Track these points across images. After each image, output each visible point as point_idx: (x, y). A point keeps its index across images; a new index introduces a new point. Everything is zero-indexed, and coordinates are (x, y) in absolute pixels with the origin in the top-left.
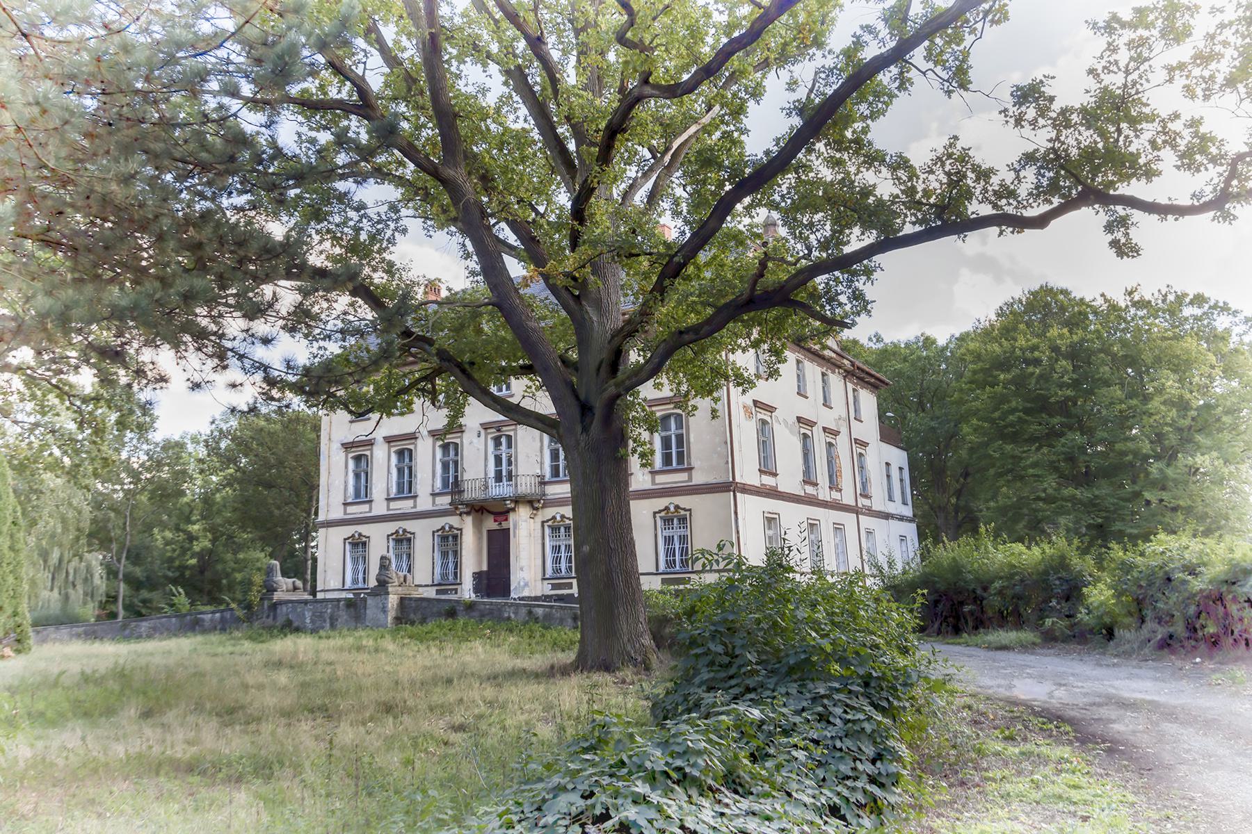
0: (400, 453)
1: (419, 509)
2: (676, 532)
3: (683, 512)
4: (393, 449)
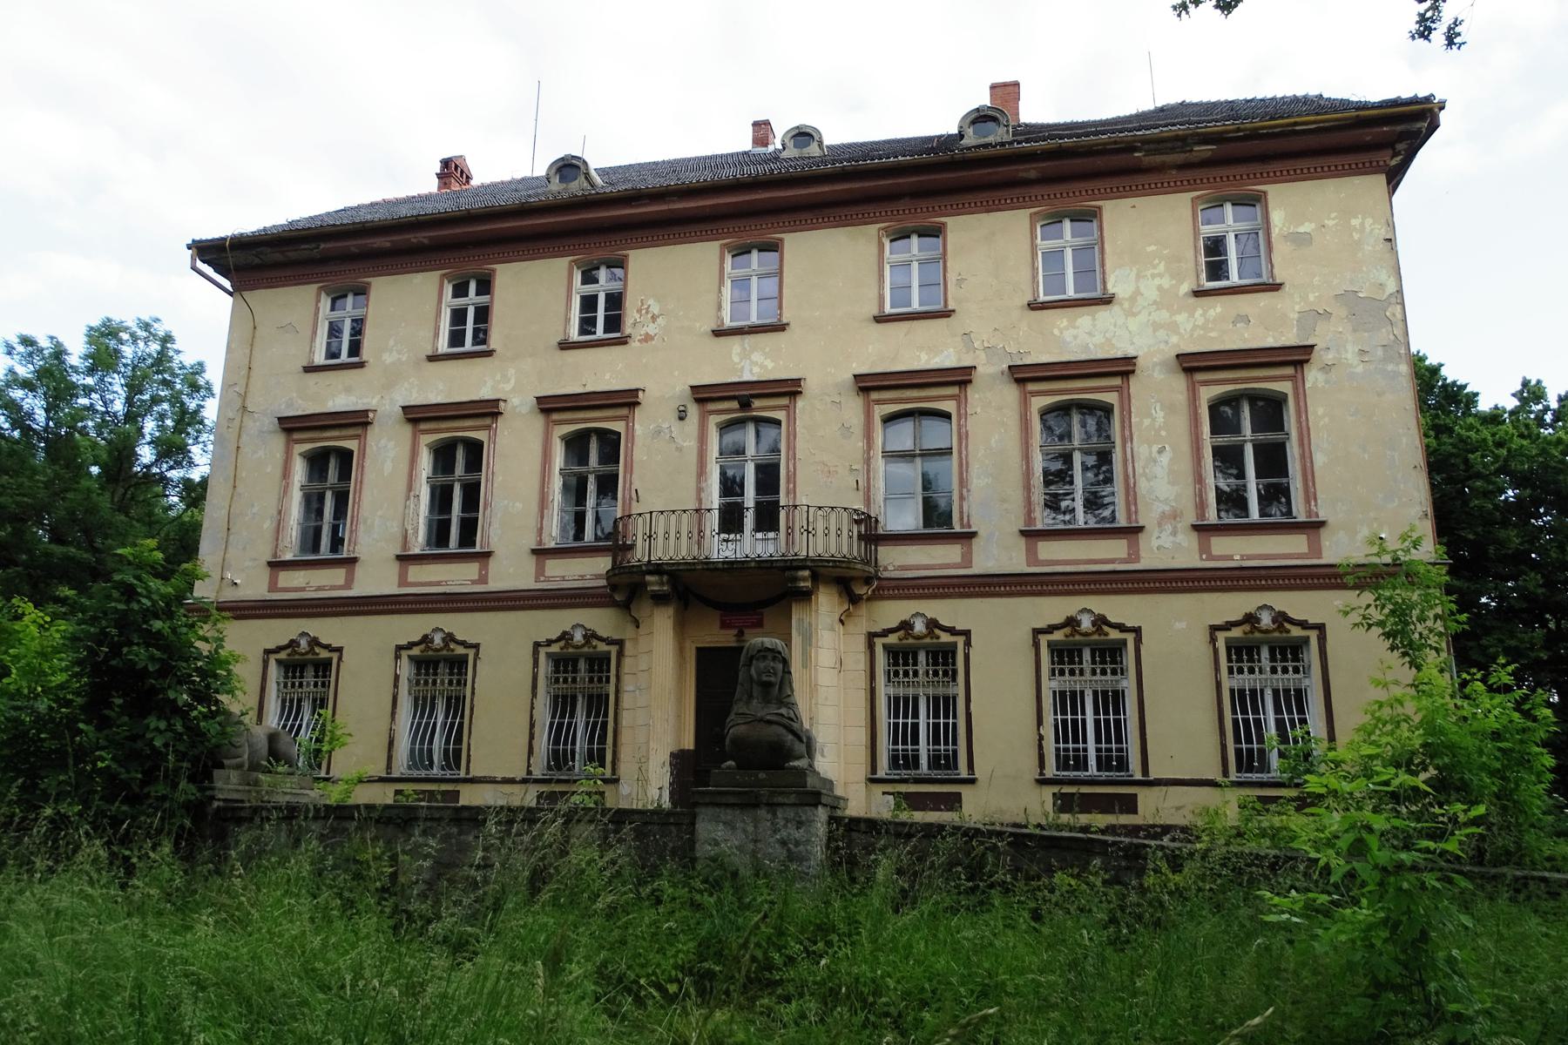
0: (317, 462)
1: (494, 585)
2: (1088, 682)
3: (602, 647)
4: (426, 439)
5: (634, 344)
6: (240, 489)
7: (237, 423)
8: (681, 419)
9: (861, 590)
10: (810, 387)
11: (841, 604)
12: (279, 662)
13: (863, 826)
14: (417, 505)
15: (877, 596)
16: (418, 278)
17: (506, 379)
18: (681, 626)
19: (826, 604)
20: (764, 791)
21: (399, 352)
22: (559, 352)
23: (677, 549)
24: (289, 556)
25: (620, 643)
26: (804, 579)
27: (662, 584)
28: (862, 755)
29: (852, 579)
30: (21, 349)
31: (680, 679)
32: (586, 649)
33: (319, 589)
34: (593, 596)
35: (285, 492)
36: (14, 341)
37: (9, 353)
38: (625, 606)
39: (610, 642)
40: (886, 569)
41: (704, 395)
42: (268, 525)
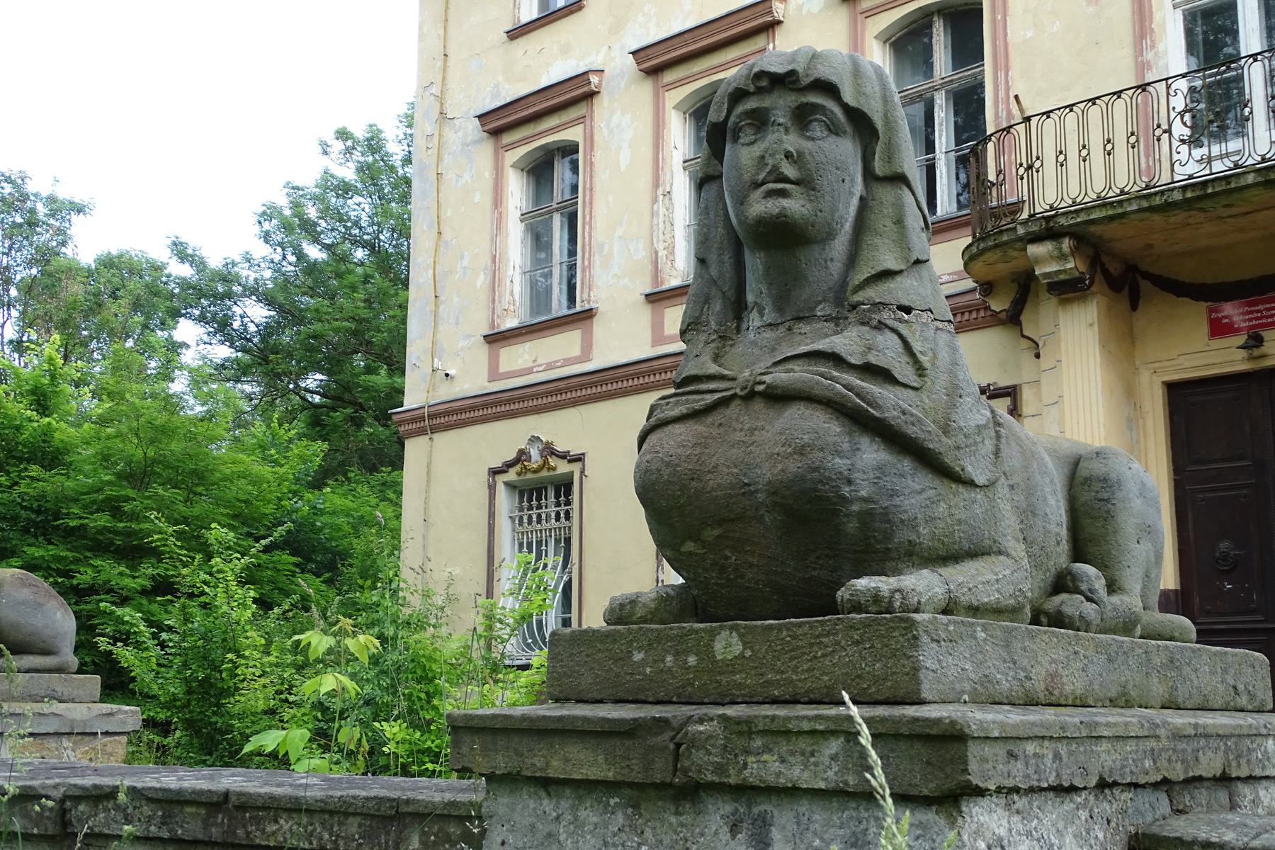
4: (675, 97)
6: (447, 235)
12: (506, 484)
18: (1123, 343)
20: (706, 723)
24: (511, 323)
25: (1011, 393)
27: (1062, 257)
30: (338, 146)
33: (550, 367)
35: (499, 228)
36: (329, 137)
37: (325, 153)
38: (1012, 319)
42: (482, 281)
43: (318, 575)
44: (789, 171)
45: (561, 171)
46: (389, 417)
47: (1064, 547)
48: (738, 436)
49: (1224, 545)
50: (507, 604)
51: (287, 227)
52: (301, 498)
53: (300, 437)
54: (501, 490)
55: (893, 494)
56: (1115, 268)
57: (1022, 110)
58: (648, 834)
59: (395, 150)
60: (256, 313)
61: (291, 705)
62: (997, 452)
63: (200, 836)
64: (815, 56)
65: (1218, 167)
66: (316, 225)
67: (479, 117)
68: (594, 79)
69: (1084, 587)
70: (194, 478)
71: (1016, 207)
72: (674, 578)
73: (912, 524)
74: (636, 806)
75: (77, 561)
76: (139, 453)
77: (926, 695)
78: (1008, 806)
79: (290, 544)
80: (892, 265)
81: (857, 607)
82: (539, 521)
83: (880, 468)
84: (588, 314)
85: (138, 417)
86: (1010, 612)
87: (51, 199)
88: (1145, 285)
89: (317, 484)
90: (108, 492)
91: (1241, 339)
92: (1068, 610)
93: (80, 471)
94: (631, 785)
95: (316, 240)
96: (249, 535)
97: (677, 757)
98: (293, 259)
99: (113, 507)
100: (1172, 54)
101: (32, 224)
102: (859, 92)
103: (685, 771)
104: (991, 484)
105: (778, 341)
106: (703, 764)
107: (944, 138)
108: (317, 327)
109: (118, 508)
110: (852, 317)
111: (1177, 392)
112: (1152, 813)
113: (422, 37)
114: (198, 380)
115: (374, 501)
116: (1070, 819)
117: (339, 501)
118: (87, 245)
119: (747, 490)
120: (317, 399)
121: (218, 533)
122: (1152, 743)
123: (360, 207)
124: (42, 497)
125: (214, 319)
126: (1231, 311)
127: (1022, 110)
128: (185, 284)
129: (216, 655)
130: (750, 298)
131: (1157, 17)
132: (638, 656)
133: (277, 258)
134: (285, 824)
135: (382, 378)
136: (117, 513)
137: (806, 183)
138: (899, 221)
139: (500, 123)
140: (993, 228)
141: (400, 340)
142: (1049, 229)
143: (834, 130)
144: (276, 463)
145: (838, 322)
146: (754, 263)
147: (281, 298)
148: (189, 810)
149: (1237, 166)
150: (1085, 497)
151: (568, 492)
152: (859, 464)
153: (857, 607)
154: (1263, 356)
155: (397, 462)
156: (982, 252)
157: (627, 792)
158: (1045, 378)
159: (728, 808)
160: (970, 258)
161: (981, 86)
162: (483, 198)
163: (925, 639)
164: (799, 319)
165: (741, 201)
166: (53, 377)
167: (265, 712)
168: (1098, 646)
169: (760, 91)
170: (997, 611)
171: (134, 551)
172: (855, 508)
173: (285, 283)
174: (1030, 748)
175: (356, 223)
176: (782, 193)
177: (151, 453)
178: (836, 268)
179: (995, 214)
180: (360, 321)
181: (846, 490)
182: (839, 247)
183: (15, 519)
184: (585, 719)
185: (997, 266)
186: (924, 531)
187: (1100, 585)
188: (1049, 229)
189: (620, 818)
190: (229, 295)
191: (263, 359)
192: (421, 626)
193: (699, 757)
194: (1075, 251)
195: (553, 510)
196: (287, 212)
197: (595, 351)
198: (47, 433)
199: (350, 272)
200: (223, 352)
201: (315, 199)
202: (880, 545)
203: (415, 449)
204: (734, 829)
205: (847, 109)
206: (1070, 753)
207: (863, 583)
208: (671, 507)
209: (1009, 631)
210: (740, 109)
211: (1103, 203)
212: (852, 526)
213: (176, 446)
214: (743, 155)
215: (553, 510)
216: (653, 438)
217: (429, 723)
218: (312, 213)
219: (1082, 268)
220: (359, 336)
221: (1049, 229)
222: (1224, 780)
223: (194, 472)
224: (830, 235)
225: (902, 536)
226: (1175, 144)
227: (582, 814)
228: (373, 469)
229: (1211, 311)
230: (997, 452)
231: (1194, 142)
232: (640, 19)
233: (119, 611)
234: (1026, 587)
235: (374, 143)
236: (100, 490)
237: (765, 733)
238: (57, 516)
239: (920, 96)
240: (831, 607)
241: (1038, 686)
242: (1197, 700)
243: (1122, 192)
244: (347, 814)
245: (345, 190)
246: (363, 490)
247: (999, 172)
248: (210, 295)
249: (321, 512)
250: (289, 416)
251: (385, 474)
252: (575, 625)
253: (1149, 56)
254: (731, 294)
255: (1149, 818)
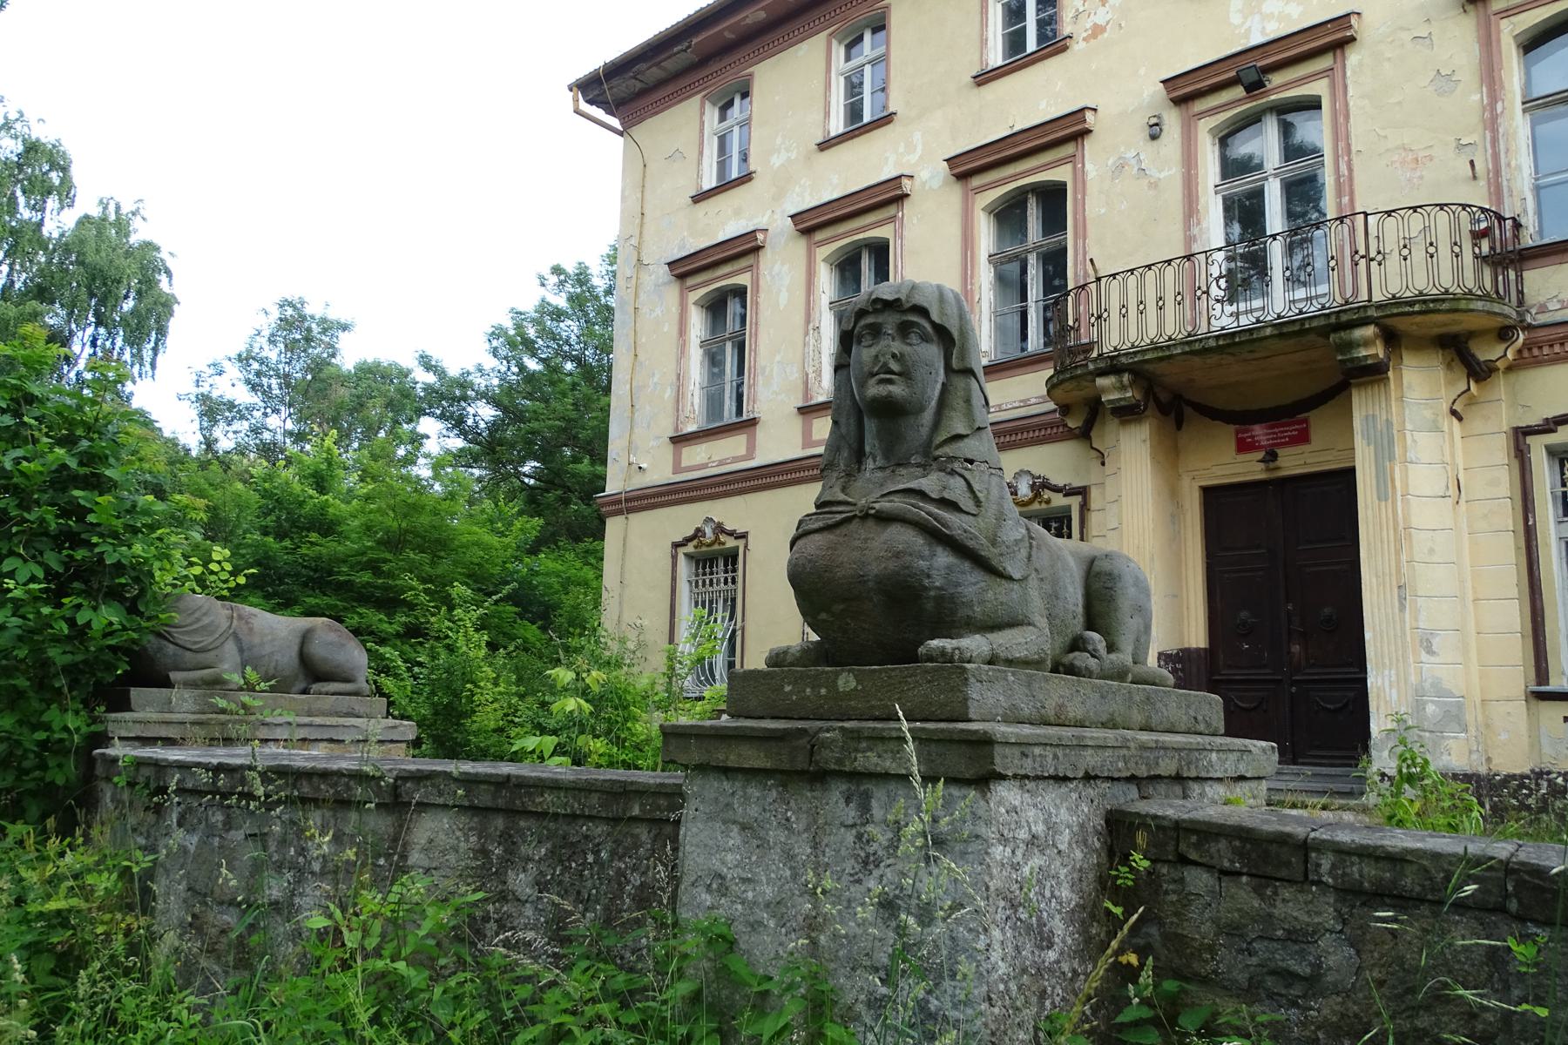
3: (1058, 500)
5: (1077, 47)
7: (634, 281)
8: (1154, 137)
9: (1488, 352)
10: (1368, 29)
11: (1450, 383)
12: (688, 556)
13: (1222, 852)
14: (818, 340)
15: (1527, 360)
16: (804, 46)
17: (910, 147)
18: (1169, 455)
19: (1420, 386)
20: (830, 732)
21: (787, 150)
22: (976, 90)
23: (1142, 327)
24: (691, 428)
25: (1083, 492)
26: (1367, 343)
27: (1123, 388)
28: (1516, 650)
29: (1471, 334)
30: (554, 279)
31: (1174, 540)
32: (1036, 506)
33: (721, 463)
34: (1040, 427)
35: (683, 352)
36: (546, 272)
38: (1084, 434)
39: (1069, 492)
40: (1543, 309)
41: (1186, 91)
42: (669, 394)
43: (533, 623)
44: (894, 366)
45: (733, 307)
46: (590, 498)
47: (1080, 619)
48: (857, 543)
49: (1244, 614)
50: (686, 648)
51: (511, 344)
52: (521, 561)
53: (520, 513)
54: (682, 560)
55: (958, 585)
56: (1164, 397)
57: (1095, 271)
58: (792, 803)
59: (599, 283)
60: (485, 413)
61: (516, 725)
62: (1029, 557)
63: (489, 804)
64: (914, 287)
65: (1245, 321)
66: (534, 342)
67: (669, 264)
68: (760, 236)
69: (1090, 648)
70: (437, 544)
71: (1089, 347)
72: (814, 637)
73: (970, 605)
74: (784, 786)
75: (345, 609)
76: (395, 524)
77: (972, 715)
78: (1021, 787)
79: (512, 598)
80: (962, 431)
81: (931, 659)
82: (711, 584)
83: (949, 568)
84: (753, 422)
85: (394, 496)
86: (1036, 664)
87: (324, 320)
88: (1188, 411)
89: (533, 550)
90: (370, 555)
91: (1260, 455)
92: (1077, 663)
93: (347, 538)
94: (782, 772)
95: (534, 355)
96: (480, 590)
97: (812, 753)
98: (515, 370)
99: (374, 567)
100: (1214, 229)
101: (308, 340)
102: (942, 313)
103: (817, 763)
104: (1025, 579)
105: (885, 479)
106: (829, 759)
107: (1035, 291)
108: (535, 425)
109: (379, 568)
110: (935, 466)
111: (1211, 495)
112: (1128, 799)
113: (623, 198)
114: (437, 466)
115: (578, 564)
116: (1064, 798)
117: (551, 565)
118: (350, 355)
119: (861, 580)
120: (532, 482)
121: (459, 590)
122: (1124, 751)
123: (570, 328)
124: (319, 558)
125: (452, 417)
126: (1259, 432)
127: (1095, 271)
128: (428, 389)
129: (457, 685)
130: (867, 449)
131: (1202, 201)
132: (788, 688)
133: (503, 369)
134: (548, 797)
135: (585, 466)
136: (377, 571)
137: (906, 375)
138: (968, 401)
139: (685, 269)
140: (1069, 360)
141: (603, 437)
142: (1113, 366)
143: (925, 338)
144: (502, 534)
145: (925, 468)
146: (870, 426)
147: (506, 401)
148: (483, 787)
149: (1258, 321)
150: (1097, 585)
151: (735, 562)
152: (936, 565)
153: (931, 659)
154: (1278, 468)
155: (599, 535)
156: (1061, 382)
157: (779, 776)
158: (1109, 481)
159: (844, 787)
160: (1052, 386)
161: (1065, 250)
162: (670, 328)
163: (972, 680)
164: (899, 465)
165: (862, 385)
166: (330, 464)
167: (494, 731)
168: (1094, 687)
169: (876, 311)
170: (1026, 663)
171: (390, 602)
172: (932, 593)
173: (509, 389)
174: (1037, 751)
175: (567, 342)
176: (890, 382)
177: (404, 525)
178: (925, 431)
179: (1072, 352)
180: (570, 420)
181: (926, 582)
182: (927, 417)
183: (297, 575)
184: (752, 729)
185: (1073, 393)
186: (977, 609)
187: (1101, 646)
188: (1113, 366)
189: (774, 793)
190: (465, 398)
191: (489, 448)
192: (619, 665)
193: (826, 753)
194: (1132, 384)
195: (722, 576)
196: (512, 332)
197: (758, 452)
198: (324, 507)
199: (561, 381)
200: (457, 443)
201: (535, 321)
202: (950, 618)
203: (613, 526)
204: (848, 801)
205: (934, 325)
206: (1065, 755)
207: (935, 643)
208: (811, 588)
209: (1028, 676)
210: (862, 323)
211: (1154, 346)
212: (930, 606)
213: (425, 520)
214: (864, 354)
215: (722, 576)
216: (800, 543)
217: (625, 740)
218: (531, 332)
219: (1138, 397)
220: (568, 432)
221: (1113, 365)
222: (1178, 778)
223: (438, 541)
224: (922, 409)
225: (963, 612)
226: (1212, 302)
227: (750, 791)
228: (577, 539)
229: (1237, 433)
230: (1029, 557)
231: (1232, 298)
232: (797, 189)
233: (382, 650)
234: (1047, 647)
235: (582, 278)
236: (364, 554)
237: (869, 738)
238: (330, 573)
239: (1016, 257)
240: (915, 659)
241: (1050, 713)
242: (1167, 726)
243: (1170, 339)
244: (590, 791)
245: (558, 315)
246: (570, 556)
247: (1076, 320)
248: (449, 398)
249: (537, 574)
250: (511, 496)
251: (587, 543)
252: (738, 666)
253: (1195, 231)
254: (855, 445)
255: (1122, 800)
